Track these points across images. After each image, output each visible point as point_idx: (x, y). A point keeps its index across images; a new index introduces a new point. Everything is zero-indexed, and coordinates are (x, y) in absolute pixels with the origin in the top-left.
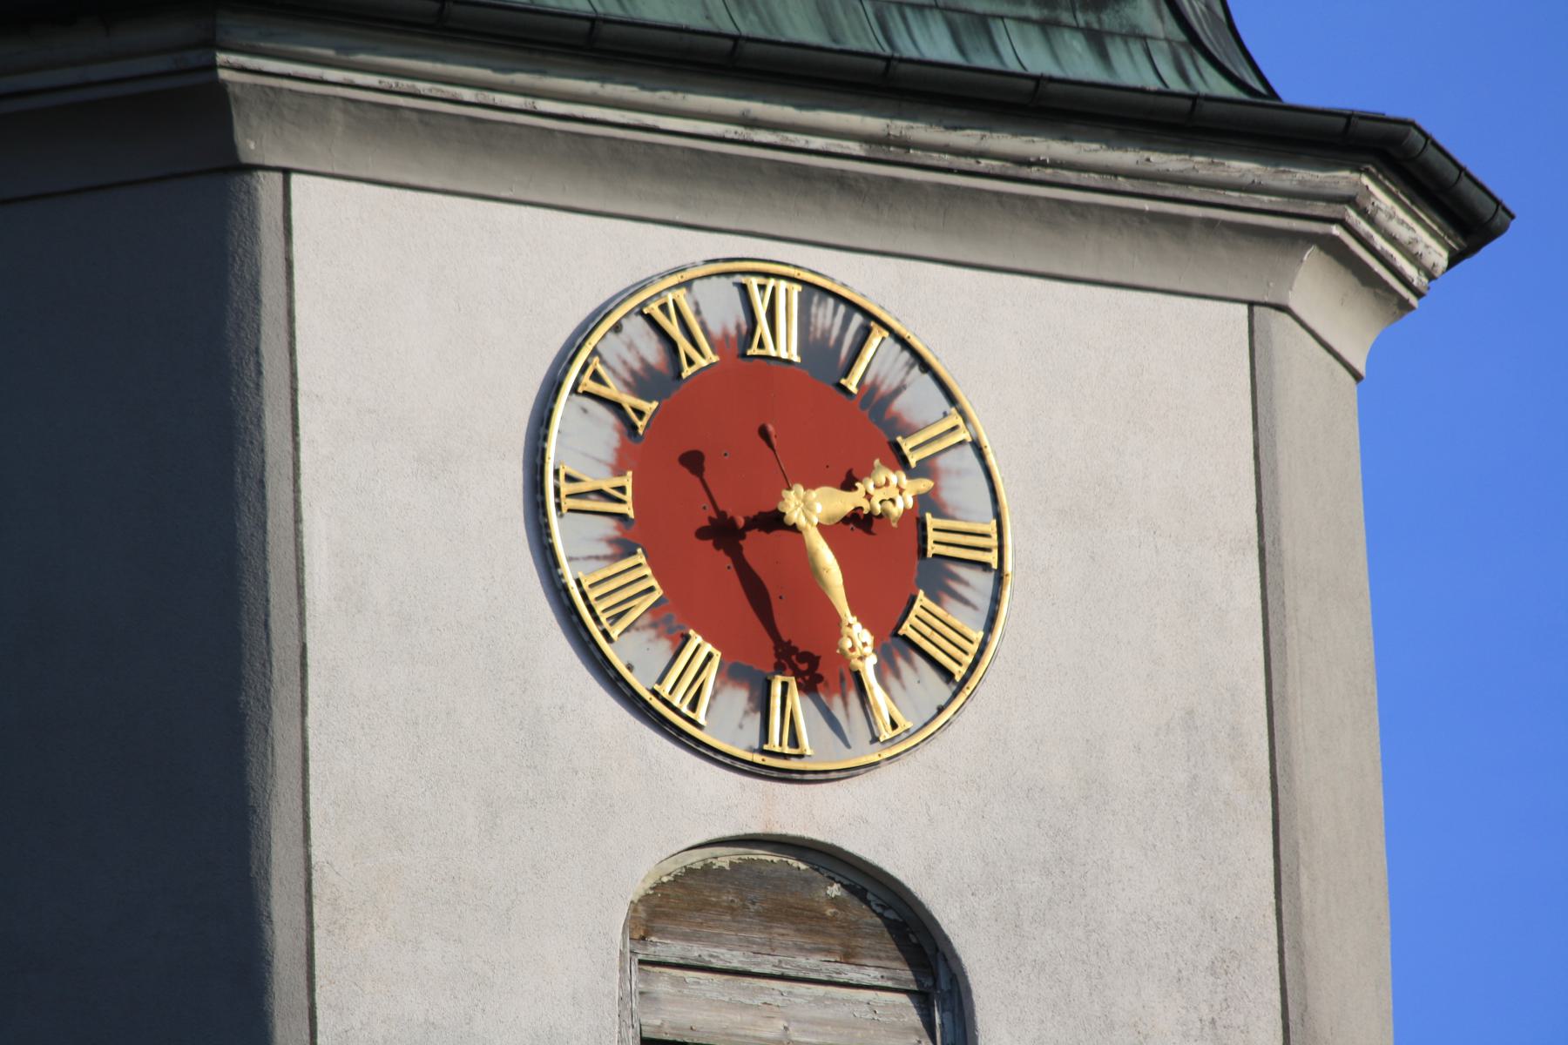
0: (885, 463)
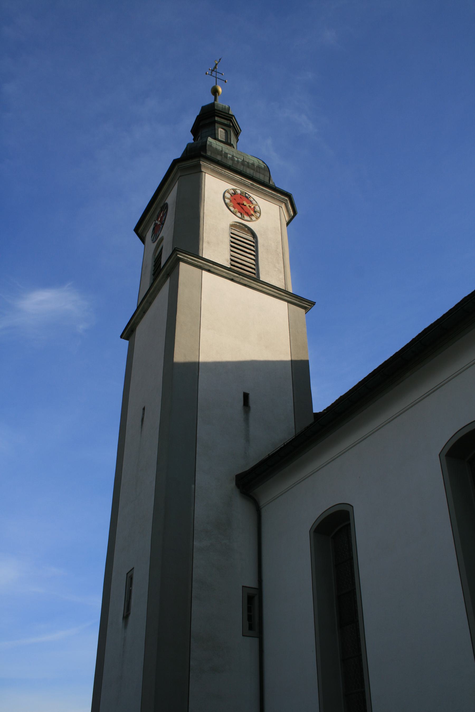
0: (239, 161)
